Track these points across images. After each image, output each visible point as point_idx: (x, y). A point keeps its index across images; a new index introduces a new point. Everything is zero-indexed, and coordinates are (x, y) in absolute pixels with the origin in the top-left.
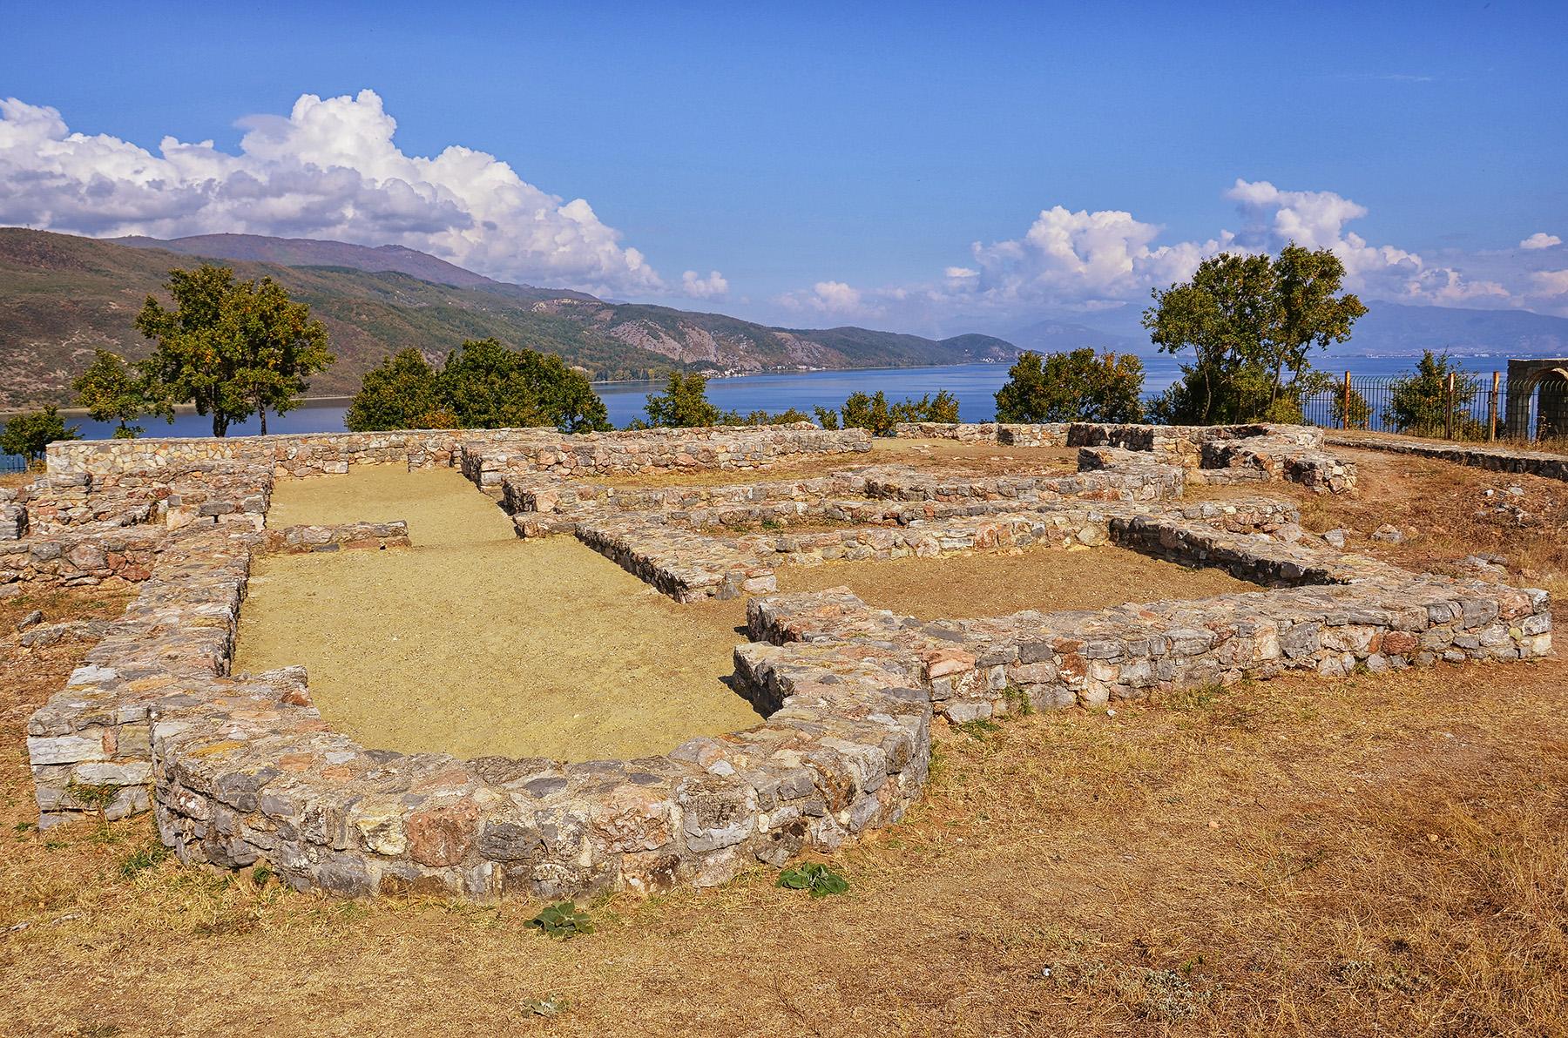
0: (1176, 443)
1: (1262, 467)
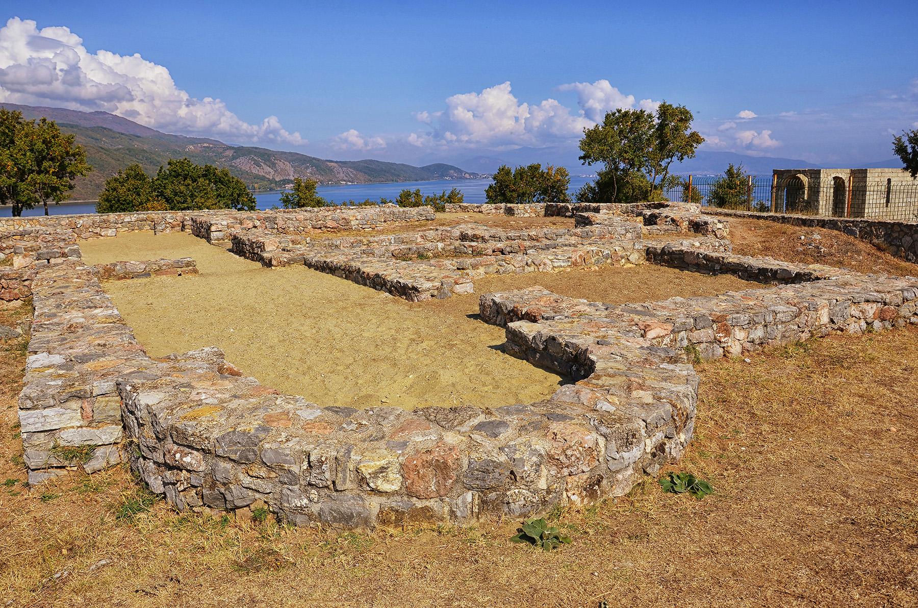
1: (677, 224)
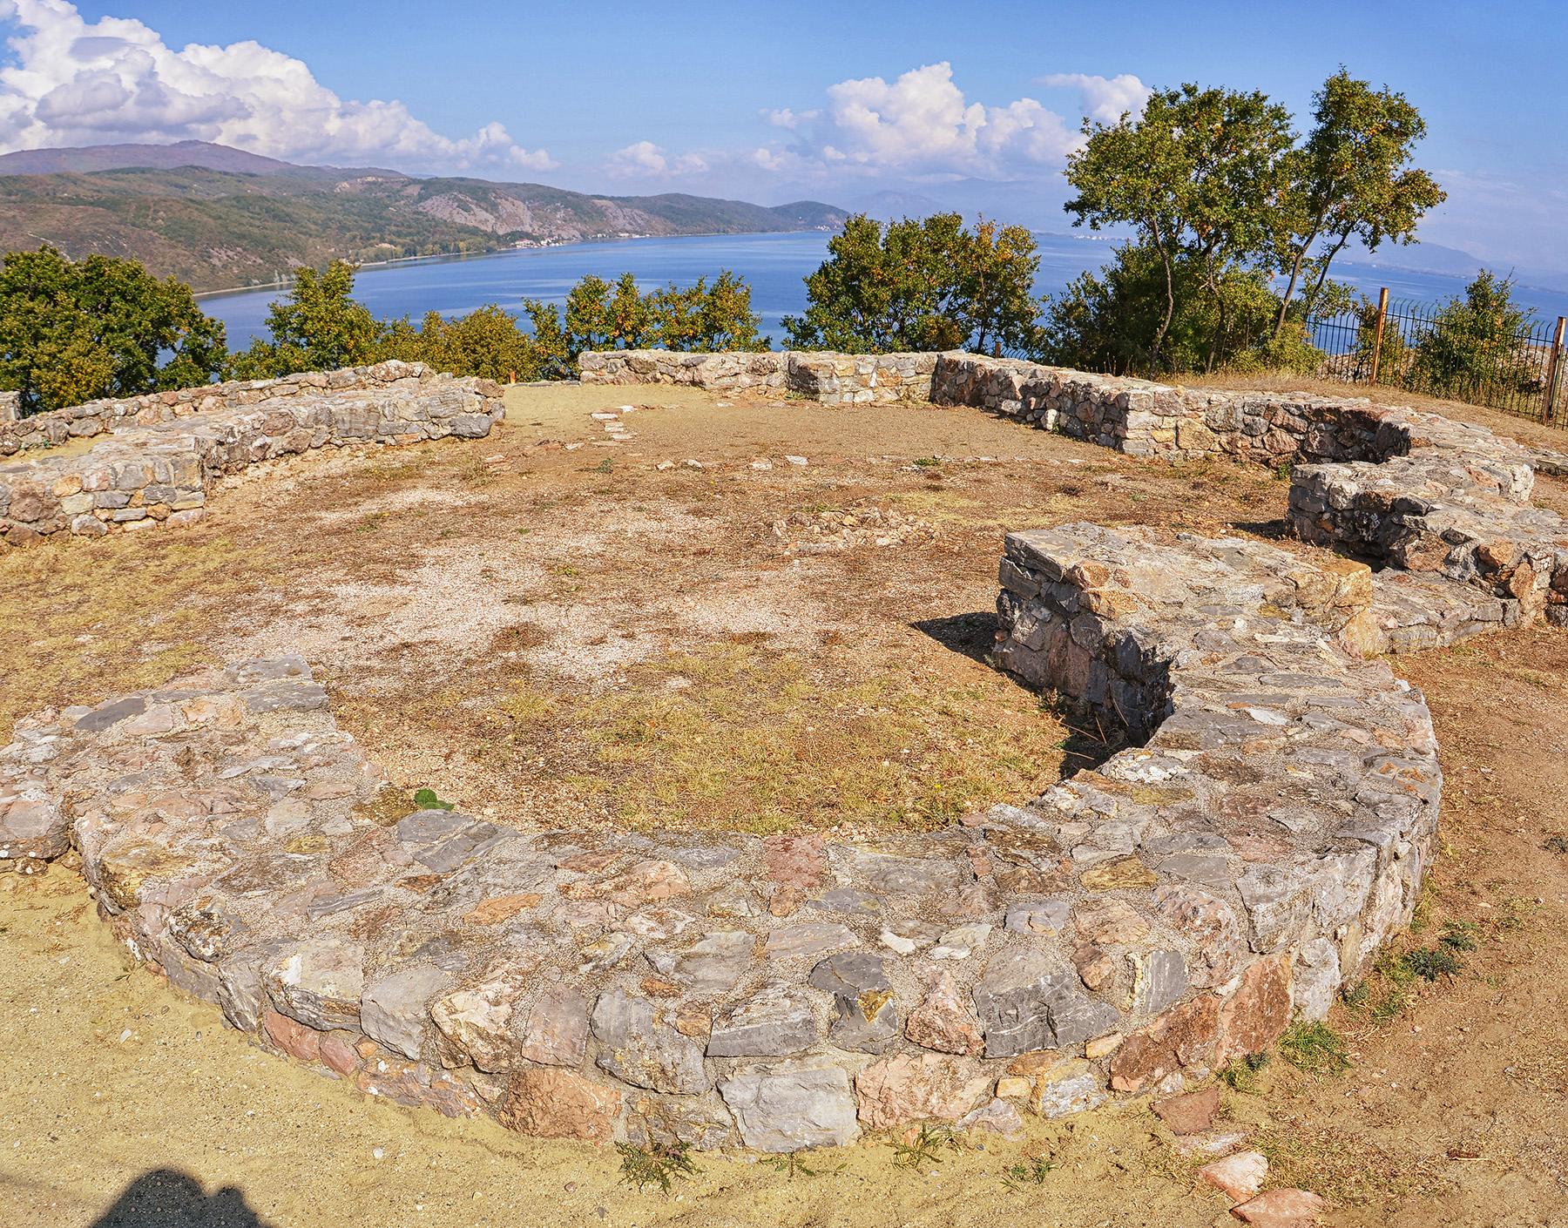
0: (1177, 428)
